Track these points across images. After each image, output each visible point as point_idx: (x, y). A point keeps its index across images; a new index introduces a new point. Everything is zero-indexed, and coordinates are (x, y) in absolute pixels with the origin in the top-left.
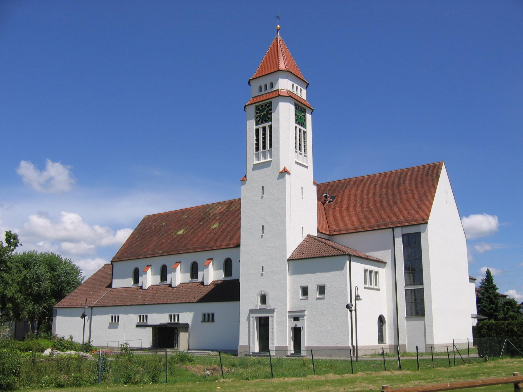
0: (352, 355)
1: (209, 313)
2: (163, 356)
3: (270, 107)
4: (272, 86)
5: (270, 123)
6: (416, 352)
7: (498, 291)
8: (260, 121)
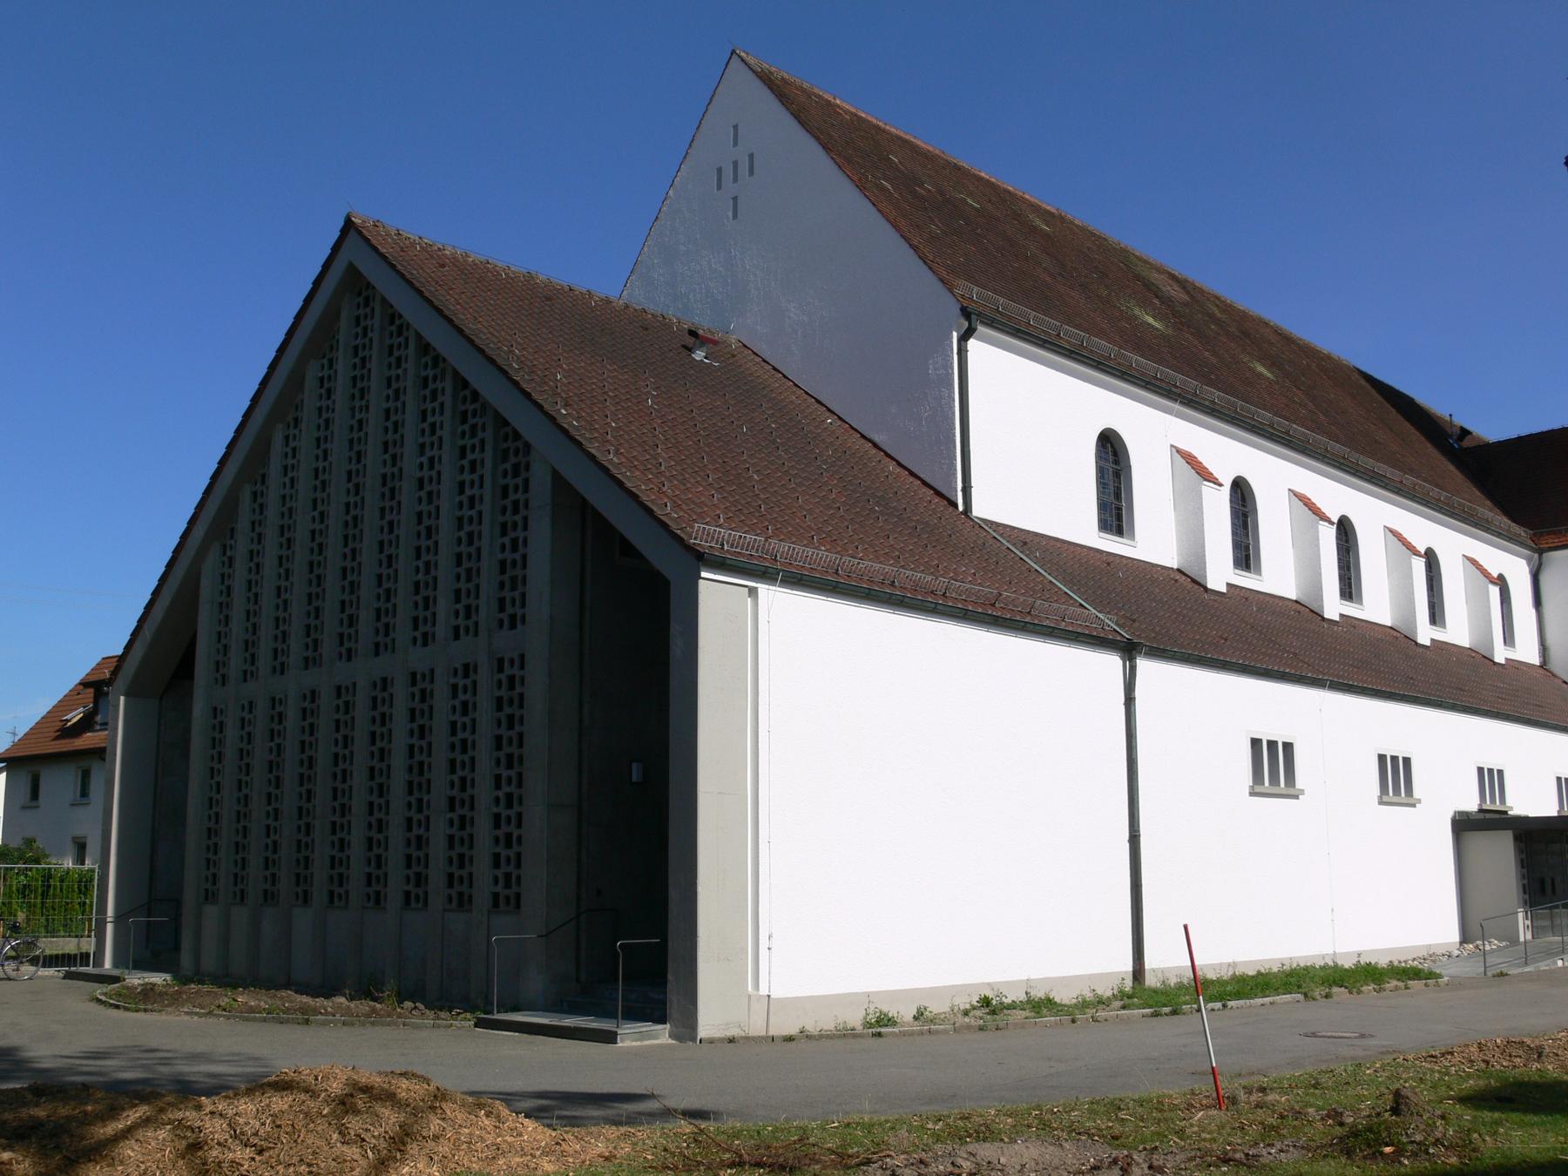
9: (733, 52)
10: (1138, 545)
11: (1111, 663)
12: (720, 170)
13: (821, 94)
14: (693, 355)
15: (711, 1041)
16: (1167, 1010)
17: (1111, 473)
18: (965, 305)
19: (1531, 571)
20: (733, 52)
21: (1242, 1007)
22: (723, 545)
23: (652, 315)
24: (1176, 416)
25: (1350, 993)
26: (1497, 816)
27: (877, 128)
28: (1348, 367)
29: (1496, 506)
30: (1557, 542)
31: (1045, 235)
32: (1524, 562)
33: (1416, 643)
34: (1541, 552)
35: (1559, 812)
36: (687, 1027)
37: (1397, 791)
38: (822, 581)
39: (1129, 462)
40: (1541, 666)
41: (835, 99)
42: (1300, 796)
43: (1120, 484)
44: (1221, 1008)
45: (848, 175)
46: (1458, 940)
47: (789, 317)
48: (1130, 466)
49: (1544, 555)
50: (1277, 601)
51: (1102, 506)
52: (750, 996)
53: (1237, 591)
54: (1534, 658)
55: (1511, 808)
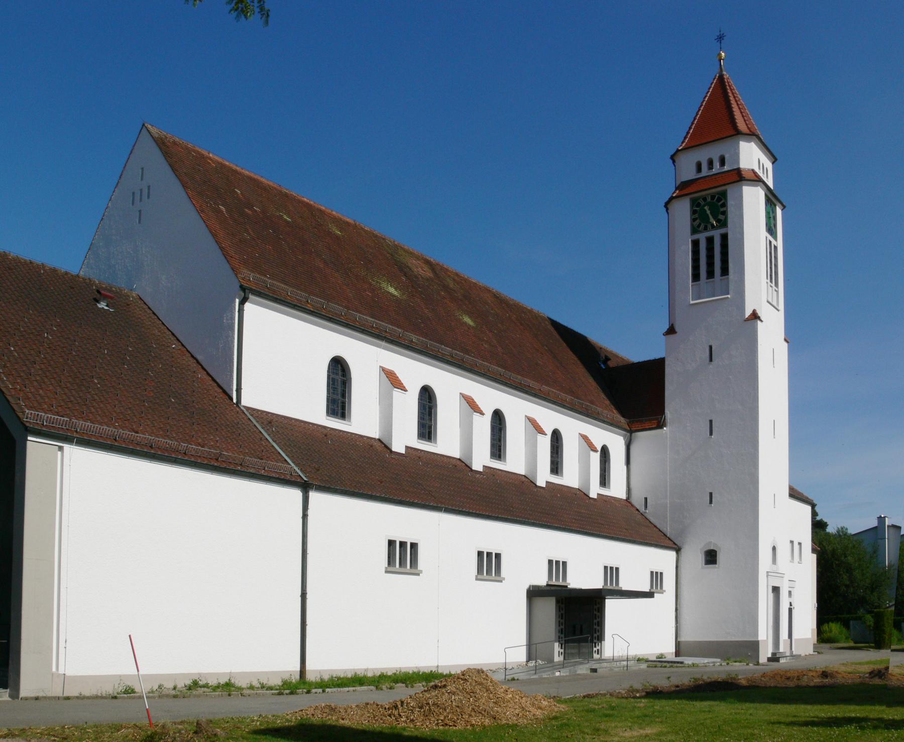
0: (555, 667)
1: (607, 565)
2: (550, 660)
3: (723, 201)
4: (722, 161)
5: (723, 231)
8: (702, 226)
9: (143, 125)
11: (296, 494)
12: (134, 193)
13: (200, 150)
14: (98, 305)
15: (26, 699)
16: (288, 691)
17: (339, 382)
18: (242, 283)
19: (625, 443)
20: (143, 125)
21: (335, 692)
22: (43, 422)
23: (83, 279)
24: (383, 349)
25: (407, 686)
26: (560, 588)
27: (236, 172)
28: (543, 318)
29: (613, 404)
31: (337, 237)
32: (622, 438)
34: (631, 432)
35: (650, 590)
36: (15, 695)
38: (98, 443)
40: (626, 500)
41: (209, 154)
42: (420, 574)
43: (345, 388)
44: (321, 692)
45: (193, 204)
46: (525, 660)
47: (162, 283)
49: (633, 434)
50: (442, 458)
51: (493, 446)
52: (53, 674)
54: (622, 495)
55: (569, 584)
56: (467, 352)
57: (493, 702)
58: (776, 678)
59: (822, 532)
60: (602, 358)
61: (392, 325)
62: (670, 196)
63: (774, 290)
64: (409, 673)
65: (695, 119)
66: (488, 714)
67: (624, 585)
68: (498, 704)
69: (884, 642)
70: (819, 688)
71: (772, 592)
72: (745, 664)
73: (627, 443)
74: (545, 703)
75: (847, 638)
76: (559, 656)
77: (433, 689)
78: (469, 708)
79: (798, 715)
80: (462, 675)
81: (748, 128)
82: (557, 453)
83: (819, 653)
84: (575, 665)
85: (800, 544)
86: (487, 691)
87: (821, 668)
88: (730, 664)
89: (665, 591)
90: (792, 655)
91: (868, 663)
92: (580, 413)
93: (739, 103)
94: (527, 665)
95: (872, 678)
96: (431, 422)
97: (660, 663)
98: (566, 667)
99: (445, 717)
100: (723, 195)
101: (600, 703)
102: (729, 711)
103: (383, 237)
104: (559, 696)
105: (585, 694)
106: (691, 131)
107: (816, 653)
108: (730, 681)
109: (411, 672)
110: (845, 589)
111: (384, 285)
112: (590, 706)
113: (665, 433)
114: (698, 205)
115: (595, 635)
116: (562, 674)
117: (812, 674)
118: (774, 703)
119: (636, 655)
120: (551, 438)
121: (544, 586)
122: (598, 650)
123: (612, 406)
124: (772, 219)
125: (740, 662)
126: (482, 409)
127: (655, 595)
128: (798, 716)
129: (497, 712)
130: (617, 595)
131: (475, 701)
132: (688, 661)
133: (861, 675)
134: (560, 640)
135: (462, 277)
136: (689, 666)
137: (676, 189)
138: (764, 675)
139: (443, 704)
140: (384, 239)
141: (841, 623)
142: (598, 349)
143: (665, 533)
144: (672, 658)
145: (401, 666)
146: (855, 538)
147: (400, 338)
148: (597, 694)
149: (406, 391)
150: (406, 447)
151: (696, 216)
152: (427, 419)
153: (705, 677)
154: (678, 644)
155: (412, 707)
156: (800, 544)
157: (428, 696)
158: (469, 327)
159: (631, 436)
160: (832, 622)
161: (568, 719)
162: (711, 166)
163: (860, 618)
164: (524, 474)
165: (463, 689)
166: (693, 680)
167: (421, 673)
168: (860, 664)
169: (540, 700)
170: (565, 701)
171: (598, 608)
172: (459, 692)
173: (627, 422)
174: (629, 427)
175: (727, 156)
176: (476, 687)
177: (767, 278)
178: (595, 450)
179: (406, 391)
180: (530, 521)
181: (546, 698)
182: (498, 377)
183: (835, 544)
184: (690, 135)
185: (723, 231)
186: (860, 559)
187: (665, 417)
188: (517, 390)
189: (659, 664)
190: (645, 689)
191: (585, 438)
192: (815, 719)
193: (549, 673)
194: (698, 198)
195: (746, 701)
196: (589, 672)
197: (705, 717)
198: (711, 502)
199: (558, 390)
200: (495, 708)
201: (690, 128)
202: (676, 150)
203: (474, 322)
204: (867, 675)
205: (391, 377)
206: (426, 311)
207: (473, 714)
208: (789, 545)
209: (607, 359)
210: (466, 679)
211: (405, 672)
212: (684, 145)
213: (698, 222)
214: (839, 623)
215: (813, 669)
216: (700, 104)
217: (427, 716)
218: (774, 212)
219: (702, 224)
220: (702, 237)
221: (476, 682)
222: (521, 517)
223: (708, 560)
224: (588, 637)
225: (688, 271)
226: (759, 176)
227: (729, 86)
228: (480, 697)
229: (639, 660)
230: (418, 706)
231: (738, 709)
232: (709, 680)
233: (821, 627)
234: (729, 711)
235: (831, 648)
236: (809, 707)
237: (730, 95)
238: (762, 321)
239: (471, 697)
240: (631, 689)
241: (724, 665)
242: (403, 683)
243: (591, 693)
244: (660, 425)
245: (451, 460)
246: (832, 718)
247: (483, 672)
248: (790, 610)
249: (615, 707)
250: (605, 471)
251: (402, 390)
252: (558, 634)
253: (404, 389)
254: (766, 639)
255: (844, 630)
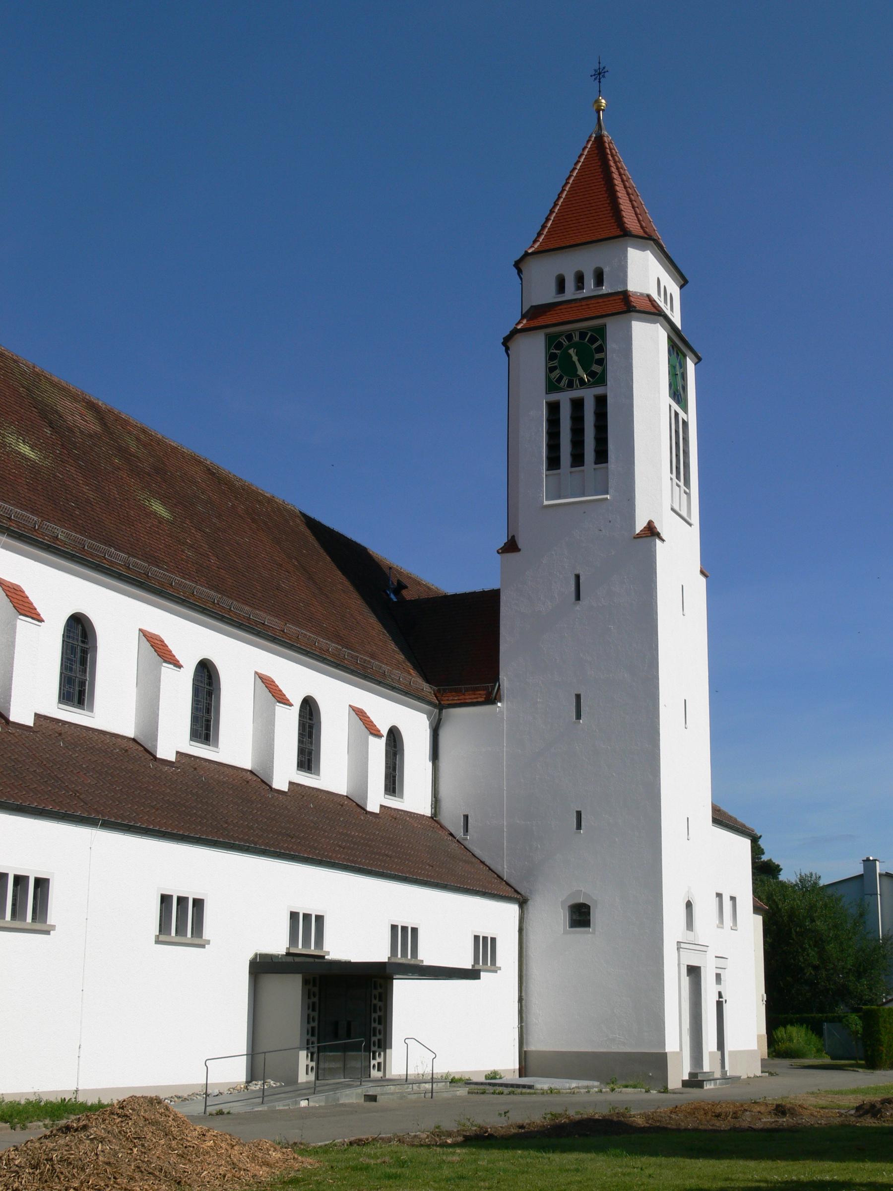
2: (292, 1079)
4: (599, 278)
5: (598, 391)
6: (205, 1083)
7: (783, 877)
8: (565, 381)
10: (322, 778)
19: (431, 724)
25: (13, 1128)
26: (311, 960)
28: (292, 513)
29: (409, 660)
30: (456, 699)
32: (425, 716)
33: (271, 787)
34: (441, 707)
35: (473, 966)
37: (180, 931)
39: (96, 644)
40: (432, 818)
42: (52, 932)
43: (211, 701)
48: (96, 647)
51: (195, 719)
53: (319, 793)
54: (424, 808)
55: (328, 953)
56: (155, 561)
57: (178, 1155)
58: (697, 1115)
59: (771, 880)
60: (393, 583)
61: (21, 508)
62: (511, 329)
63: (682, 491)
64: (19, 1104)
65: (555, 204)
66: (166, 1176)
67: (428, 956)
68: (186, 1158)
69: (881, 1058)
70: (771, 1132)
71: (687, 976)
72: (644, 1090)
73: (434, 725)
74: (275, 1155)
75: (818, 1051)
76: (307, 1073)
77: (63, 1132)
78: (130, 1165)
79: (733, 1177)
80: (119, 1108)
81: (642, 227)
82: (310, 736)
83: (771, 1074)
84: (337, 1089)
85: (733, 899)
86: (166, 1135)
87: (774, 1099)
88: (617, 1089)
89: (500, 968)
90: (724, 1077)
91: (854, 1092)
92: (352, 672)
93: (627, 184)
94: (246, 1088)
95: (860, 1116)
96: (85, 676)
97: (491, 1087)
98: (320, 1092)
99: (82, 1183)
100: (601, 332)
101: (378, 1154)
102: (612, 1170)
103: (15, 358)
104: (302, 1142)
105: (352, 1139)
106: (549, 225)
107: (767, 1074)
108: (615, 1119)
109: (23, 1102)
110: (813, 973)
111: (11, 439)
112: (361, 1160)
113: (500, 711)
114: (559, 346)
115: (374, 1039)
116: (312, 1104)
117: (758, 1109)
118: (691, 1157)
119: (448, 1074)
120: (300, 711)
121: (282, 955)
122: (379, 1064)
123: (409, 664)
124: (679, 377)
125: (635, 1087)
126: (178, 657)
127: (482, 974)
128: (732, 1180)
129: (185, 1172)
130: (413, 973)
131: (142, 1152)
132: (543, 1084)
133: (843, 1111)
134: (310, 1046)
135: (152, 436)
136: (543, 1093)
137: (523, 316)
138: (675, 1110)
139: (80, 1159)
140: (15, 361)
141: (807, 1027)
142: (387, 571)
143: (501, 875)
144: (514, 1078)
145: (4, 1092)
146: (830, 891)
147: (35, 530)
148: (374, 1139)
149: (41, 621)
150: (36, 715)
151: (555, 363)
152: (78, 669)
153: (572, 1113)
154: (524, 1056)
155: (17, 1166)
156: (733, 899)
157: (51, 1145)
158: (161, 520)
159: (440, 713)
160: (792, 1024)
161: (319, 1183)
162: (580, 284)
163: (840, 1019)
164: (250, 769)
165: (120, 1132)
166: (549, 1116)
167: (42, 1103)
168: (840, 1093)
169: (268, 1150)
170: (315, 1152)
171: (380, 995)
172: (112, 1139)
173: (434, 691)
174: (437, 699)
175: (606, 270)
176: (145, 1129)
177: (671, 472)
178: (378, 735)
179: (41, 621)
180: (258, 846)
181: (278, 1147)
182: (209, 606)
183: (794, 900)
184: (546, 230)
185: (598, 391)
186: (836, 926)
187: (499, 686)
188: (242, 629)
189: (491, 1089)
190: (463, 1131)
191: (360, 713)
192: (763, 1185)
193: (287, 1102)
194: (560, 334)
195: (643, 1153)
196: (362, 1100)
197: (569, 1180)
198: (579, 826)
199: (314, 633)
200: (181, 1165)
201: (547, 219)
202: (524, 253)
203: (171, 512)
204: (853, 1112)
205: (14, 596)
206: (85, 489)
207: (137, 1176)
208: (715, 901)
209: (401, 586)
210: (127, 1116)
211: (11, 1102)
212: (536, 246)
213: (557, 373)
214: (805, 1026)
215: (762, 1100)
216: (564, 182)
217: (46, 1181)
218: (683, 366)
219: (565, 378)
220: (565, 398)
221: (146, 1120)
222: (240, 840)
223: (574, 920)
224: (362, 1042)
225: (541, 452)
226: (659, 306)
227: (613, 156)
228: (152, 1146)
229: (453, 1081)
230: (31, 1164)
231: (627, 1166)
232: (578, 1117)
233: (774, 1033)
234: (612, 1170)
235: (792, 1067)
236: (752, 1164)
237: (614, 169)
238: (663, 540)
239: (135, 1147)
240: (437, 1130)
241: (607, 1092)
242: (6, 1122)
243: (363, 1137)
244: (491, 699)
245: (119, 740)
246: (792, 1182)
247: (160, 1102)
248: (720, 1005)
249: (406, 1162)
250: (394, 769)
251: (33, 618)
252: (306, 1037)
253: (38, 618)
254: (678, 1050)
255: (814, 1038)
